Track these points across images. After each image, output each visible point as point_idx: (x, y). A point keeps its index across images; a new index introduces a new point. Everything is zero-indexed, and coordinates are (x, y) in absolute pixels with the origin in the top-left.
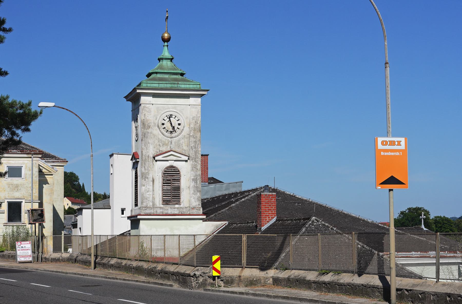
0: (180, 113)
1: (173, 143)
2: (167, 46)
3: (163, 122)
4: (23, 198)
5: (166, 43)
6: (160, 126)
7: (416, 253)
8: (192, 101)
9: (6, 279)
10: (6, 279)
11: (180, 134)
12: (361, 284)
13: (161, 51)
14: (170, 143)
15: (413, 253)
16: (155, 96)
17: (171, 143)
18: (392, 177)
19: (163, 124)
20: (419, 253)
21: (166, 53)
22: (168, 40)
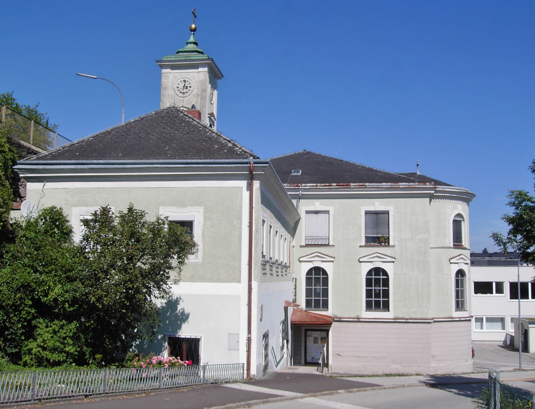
0: (191, 79)
1: (185, 101)
2: (193, 34)
3: (178, 86)
4: (52, 129)
5: (192, 33)
6: (175, 89)
7: (387, 184)
8: (200, 69)
9: (295, 193)
10: (295, 193)
11: (191, 94)
12: (518, 191)
13: (189, 39)
14: (182, 101)
15: (384, 184)
16: (173, 67)
17: (184, 101)
18: (474, 356)
19: (178, 87)
20: (390, 184)
21: (192, 39)
22: (194, 30)
